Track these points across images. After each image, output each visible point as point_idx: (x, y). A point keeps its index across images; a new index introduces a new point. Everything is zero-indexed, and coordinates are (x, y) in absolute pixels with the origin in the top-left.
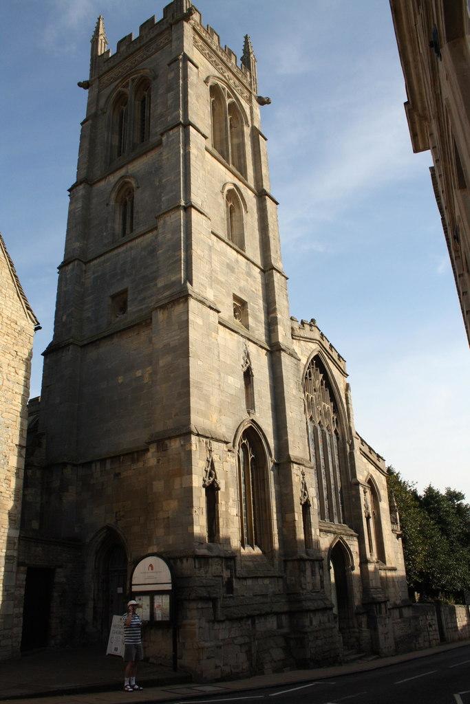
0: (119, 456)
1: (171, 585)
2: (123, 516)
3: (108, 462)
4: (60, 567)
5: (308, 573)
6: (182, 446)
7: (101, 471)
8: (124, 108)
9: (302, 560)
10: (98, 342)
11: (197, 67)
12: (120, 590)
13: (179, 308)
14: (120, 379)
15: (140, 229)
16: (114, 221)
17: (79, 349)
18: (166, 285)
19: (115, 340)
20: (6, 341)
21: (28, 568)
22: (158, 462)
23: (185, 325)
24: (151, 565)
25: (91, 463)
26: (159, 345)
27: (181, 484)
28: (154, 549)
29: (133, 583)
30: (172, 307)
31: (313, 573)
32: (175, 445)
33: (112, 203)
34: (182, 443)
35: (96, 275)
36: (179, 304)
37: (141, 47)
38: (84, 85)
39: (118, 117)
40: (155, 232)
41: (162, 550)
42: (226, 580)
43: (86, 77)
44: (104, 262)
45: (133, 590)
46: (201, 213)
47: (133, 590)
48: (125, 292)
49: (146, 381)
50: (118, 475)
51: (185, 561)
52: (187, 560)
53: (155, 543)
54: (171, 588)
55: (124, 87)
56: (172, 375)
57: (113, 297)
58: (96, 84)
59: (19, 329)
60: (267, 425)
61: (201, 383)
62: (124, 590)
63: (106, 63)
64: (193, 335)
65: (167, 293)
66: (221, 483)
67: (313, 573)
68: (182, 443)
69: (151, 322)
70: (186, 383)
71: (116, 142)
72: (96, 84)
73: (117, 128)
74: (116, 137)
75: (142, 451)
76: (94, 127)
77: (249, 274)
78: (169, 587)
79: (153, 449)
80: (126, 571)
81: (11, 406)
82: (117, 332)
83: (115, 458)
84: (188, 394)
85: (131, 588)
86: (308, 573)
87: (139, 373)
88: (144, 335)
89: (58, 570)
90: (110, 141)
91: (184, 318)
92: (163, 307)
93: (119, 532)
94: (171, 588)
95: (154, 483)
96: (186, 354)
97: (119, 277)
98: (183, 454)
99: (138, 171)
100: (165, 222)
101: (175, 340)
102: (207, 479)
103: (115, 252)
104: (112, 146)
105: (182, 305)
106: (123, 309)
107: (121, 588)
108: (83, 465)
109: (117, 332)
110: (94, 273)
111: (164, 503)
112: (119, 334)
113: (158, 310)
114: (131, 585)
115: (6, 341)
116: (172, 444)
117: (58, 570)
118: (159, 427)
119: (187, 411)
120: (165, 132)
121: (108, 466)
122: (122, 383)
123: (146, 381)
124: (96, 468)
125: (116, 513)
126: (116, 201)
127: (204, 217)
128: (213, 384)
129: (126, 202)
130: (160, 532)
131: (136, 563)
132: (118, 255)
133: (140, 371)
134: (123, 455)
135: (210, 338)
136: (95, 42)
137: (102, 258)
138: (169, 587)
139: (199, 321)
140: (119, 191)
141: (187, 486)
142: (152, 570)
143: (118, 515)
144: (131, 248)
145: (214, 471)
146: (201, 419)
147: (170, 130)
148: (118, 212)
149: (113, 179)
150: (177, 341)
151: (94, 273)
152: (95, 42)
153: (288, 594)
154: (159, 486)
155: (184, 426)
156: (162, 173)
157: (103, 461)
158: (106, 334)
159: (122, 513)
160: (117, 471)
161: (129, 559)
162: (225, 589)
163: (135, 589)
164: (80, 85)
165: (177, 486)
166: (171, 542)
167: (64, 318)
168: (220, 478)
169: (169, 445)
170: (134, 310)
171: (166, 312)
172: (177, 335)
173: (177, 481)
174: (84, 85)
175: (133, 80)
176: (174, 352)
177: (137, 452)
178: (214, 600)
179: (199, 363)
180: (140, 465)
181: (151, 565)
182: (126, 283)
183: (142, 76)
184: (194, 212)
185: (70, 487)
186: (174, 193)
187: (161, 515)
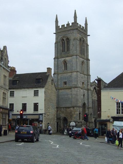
5: (91, 124)
9: (90, 122)
31: (91, 124)
33: (63, 64)
43: (55, 32)
46: (100, 142)
60: (86, 102)
67: (91, 124)
77: (85, 77)
79: (72, 108)
86: (91, 124)
87: (69, 96)
88: (70, 90)
100: (73, 74)
118: (73, 105)
121: (64, 109)
129: (65, 64)
130: (73, 118)
132: (64, 75)
136: (57, 21)
152: (57, 21)
153: (57, 108)
154: (73, 113)
158: (63, 88)
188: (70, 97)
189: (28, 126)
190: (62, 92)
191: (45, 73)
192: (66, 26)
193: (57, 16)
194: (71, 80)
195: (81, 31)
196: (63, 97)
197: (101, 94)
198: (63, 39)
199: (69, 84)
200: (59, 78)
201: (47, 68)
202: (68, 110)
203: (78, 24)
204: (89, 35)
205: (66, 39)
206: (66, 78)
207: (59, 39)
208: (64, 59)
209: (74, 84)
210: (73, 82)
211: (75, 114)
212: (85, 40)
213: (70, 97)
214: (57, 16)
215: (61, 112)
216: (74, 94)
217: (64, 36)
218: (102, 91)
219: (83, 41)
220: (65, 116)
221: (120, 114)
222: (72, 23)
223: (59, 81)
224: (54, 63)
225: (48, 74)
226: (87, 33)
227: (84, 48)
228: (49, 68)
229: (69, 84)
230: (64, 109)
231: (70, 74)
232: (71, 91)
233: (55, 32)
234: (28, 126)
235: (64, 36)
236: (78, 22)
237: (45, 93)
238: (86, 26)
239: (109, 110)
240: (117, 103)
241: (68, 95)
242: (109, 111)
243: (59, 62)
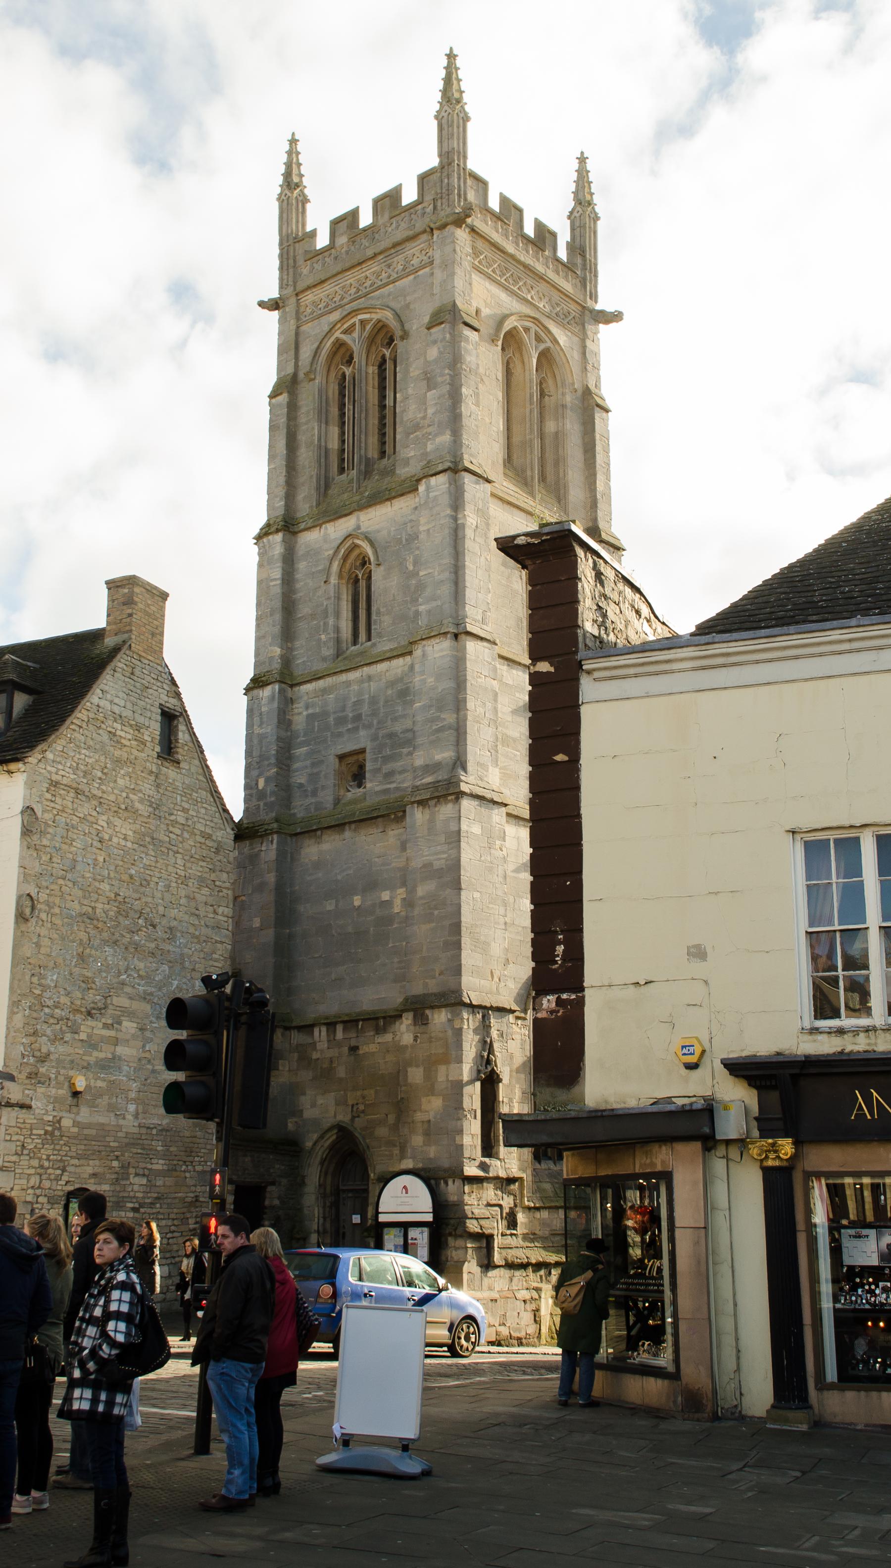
0: (357, 1021)
1: (431, 1215)
2: (363, 1112)
3: (340, 1028)
4: (273, 1183)
6: (449, 1020)
7: (329, 1041)
8: (348, 371)
10: (319, 833)
11: (476, 330)
12: (356, 1219)
13: (446, 810)
14: (357, 901)
15: (384, 646)
16: (337, 615)
17: (289, 838)
18: (427, 766)
19: (348, 834)
20: (201, 869)
21: (237, 1187)
22: (415, 1040)
23: (455, 839)
24: (405, 1187)
25: (312, 1026)
26: (417, 863)
27: (447, 1076)
28: (408, 1164)
29: (380, 1210)
30: (435, 806)
32: (439, 1018)
33: (333, 580)
34: (449, 1017)
35: (310, 711)
36: (446, 803)
37: (375, 255)
38: (273, 305)
39: (337, 387)
40: (408, 659)
41: (420, 1165)
42: (507, 1210)
44: (325, 691)
45: (380, 1220)
47: (380, 1220)
48: (363, 751)
49: (396, 910)
50: (354, 1049)
51: (450, 1182)
52: (454, 1181)
53: (409, 1155)
54: (431, 1220)
55: (345, 332)
56: (436, 912)
57: (341, 757)
58: (290, 308)
59: (215, 845)
61: (476, 926)
62: (364, 1218)
63: (308, 262)
64: (468, 855)
65: (429, 779)
66: (504, 1070)
68: (449, 1017)
69: (404, 816)
70: (456, 928)
71: (334, 444)
72: (290, 308)
73: (334, 411)
74: (335, 431)
75: (391, 1017)
76: (292, 407)
78: (429, 1218)
79: (407, 1020)
80: (366, 1191)
81: (211, 963)
82: (350, 823)
83: (351, 1022)
84: (458, 946)
85: (377, 1217)
87: (386, 896)
88: (393, 834)
89: (270, 1188)
90: (323, 444)
91: (453, 827)
92: (422, 803)
93: (357, 1135)
94: (431, 1220)
95: (409, 1069)
96: (457, 887)
97: (350, 726)
98: (450, 1033)
99: (378, 531)
101: (440, 859)
102: (482, 1068)
103: (344, 677)
104: (327, 451)
105: (450, 806)
106: (359, 777)
107: (359, 1216)
108: (300, 1028)
109: (350, 823)
110: (307, 708)
111: (424, 1100)
112: (353, 826)
113: (416, 805)
114: (377, 1213)
115: (201, 869)
116: (436, 1016)
117: (270, 1188)
118: (417, 989)
119: (457, 971)
120: (425, 477)
121: (340, 1034)
122: (359, 907)
123: (396, 910)
124: (320, 1034)
125: (353, 1106)
126: (340, 576)
127: (485, 644)
128: (496, 923)
130: (417, 1140)
131: (386, 1180)
132: (348, 684)
133: (388, 892)
134: (363, 1020)
135: (493, 851)
137: (321, 683)
138: (429, 1218)
139: (476, 829)
140: (345, 558)
141: (456, 1078)
142: (407, 1193)
143: (355, 1109)
144: (370, 678)
145: (494, 1055)
146: (477, 981)
147: (432, 475)
148: (344, 597)
149: (336, 530)
150: (443, 861)
151: (307, 708)
154: (416, 1075)
155: (453, 992)
156: (418, 548)
157: (331, 1025)
159: (362, 1107)
160: (353, 1043)
161: (372, 1175)
162: (505, 1222)
163: (382, 1218)
164: (262, 304)
165: (441, 1078)
166: (432, 1155)
167: (261, 783)
168: (503, 1065)
169: (430, 1017)
170: (378, 789)
171: (427, 811)
172: (444, 852)
173: (442, 1069)
174: (273, 305)
175: (362, 322)
176: (439, 878)
177: (384, 1018)
178: (489, 1238)
179: (477, 895)
180: (388, 1037)
181: (405, 1187)
182: (362, 739)
183: (379, 321)
184: (471, 646)
185: (280, 1062)
186: (439, 603)
187: (419, 1116)
188: (388, 904)
189: (666, 1273)
190: (317, 865)
191: (95, 636)
192: (366, 219)
193: (293, 152)
194: (408, 724)
195: (527, 257)
196: (330, 906)
197: (577, 733)
198: (339, 345)
199: (386, 768)
200: (299, 720)
201: (107, 583)
202: (372, 1048)
203: (482, 184)
204: (615, 317)
205: (371, 341)
206: (365, 709)
207: (306, 353)
208: (345, 525)
209: (429, 768)
210: (419, 741)
211: (431, 1091)
212: (574, 356)
213: (388, 904)
214: (293, 152)
215: (306, 1075)
216: (428, 865)
217: (355, 312)
218: (588, 688)
219: (546, 357)
220: (344, 1117)
221: (868, 1011)
222: (423, 179)
223: (301, 751)
224: (260, 583)
225: (110, 641)
226: (594, 297)
227: (557, 433)
228: (131, 581)
229: (386, 768)
230: (340, 1034)
231: (399, 664)
232: (403, 847)
233: (274, 293)
234: (666, 1273)
235: (355, 312)
236: (472, 164)
237: (26, 832)
238: (582, 227)
239: (698, 953)
240: (809, 846)
241: (372, 885)
242: (698, 968)
243: (302, 566)
